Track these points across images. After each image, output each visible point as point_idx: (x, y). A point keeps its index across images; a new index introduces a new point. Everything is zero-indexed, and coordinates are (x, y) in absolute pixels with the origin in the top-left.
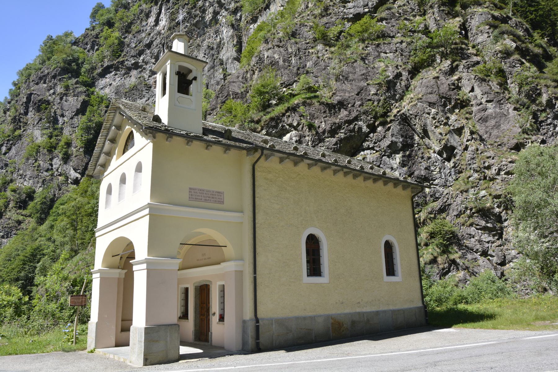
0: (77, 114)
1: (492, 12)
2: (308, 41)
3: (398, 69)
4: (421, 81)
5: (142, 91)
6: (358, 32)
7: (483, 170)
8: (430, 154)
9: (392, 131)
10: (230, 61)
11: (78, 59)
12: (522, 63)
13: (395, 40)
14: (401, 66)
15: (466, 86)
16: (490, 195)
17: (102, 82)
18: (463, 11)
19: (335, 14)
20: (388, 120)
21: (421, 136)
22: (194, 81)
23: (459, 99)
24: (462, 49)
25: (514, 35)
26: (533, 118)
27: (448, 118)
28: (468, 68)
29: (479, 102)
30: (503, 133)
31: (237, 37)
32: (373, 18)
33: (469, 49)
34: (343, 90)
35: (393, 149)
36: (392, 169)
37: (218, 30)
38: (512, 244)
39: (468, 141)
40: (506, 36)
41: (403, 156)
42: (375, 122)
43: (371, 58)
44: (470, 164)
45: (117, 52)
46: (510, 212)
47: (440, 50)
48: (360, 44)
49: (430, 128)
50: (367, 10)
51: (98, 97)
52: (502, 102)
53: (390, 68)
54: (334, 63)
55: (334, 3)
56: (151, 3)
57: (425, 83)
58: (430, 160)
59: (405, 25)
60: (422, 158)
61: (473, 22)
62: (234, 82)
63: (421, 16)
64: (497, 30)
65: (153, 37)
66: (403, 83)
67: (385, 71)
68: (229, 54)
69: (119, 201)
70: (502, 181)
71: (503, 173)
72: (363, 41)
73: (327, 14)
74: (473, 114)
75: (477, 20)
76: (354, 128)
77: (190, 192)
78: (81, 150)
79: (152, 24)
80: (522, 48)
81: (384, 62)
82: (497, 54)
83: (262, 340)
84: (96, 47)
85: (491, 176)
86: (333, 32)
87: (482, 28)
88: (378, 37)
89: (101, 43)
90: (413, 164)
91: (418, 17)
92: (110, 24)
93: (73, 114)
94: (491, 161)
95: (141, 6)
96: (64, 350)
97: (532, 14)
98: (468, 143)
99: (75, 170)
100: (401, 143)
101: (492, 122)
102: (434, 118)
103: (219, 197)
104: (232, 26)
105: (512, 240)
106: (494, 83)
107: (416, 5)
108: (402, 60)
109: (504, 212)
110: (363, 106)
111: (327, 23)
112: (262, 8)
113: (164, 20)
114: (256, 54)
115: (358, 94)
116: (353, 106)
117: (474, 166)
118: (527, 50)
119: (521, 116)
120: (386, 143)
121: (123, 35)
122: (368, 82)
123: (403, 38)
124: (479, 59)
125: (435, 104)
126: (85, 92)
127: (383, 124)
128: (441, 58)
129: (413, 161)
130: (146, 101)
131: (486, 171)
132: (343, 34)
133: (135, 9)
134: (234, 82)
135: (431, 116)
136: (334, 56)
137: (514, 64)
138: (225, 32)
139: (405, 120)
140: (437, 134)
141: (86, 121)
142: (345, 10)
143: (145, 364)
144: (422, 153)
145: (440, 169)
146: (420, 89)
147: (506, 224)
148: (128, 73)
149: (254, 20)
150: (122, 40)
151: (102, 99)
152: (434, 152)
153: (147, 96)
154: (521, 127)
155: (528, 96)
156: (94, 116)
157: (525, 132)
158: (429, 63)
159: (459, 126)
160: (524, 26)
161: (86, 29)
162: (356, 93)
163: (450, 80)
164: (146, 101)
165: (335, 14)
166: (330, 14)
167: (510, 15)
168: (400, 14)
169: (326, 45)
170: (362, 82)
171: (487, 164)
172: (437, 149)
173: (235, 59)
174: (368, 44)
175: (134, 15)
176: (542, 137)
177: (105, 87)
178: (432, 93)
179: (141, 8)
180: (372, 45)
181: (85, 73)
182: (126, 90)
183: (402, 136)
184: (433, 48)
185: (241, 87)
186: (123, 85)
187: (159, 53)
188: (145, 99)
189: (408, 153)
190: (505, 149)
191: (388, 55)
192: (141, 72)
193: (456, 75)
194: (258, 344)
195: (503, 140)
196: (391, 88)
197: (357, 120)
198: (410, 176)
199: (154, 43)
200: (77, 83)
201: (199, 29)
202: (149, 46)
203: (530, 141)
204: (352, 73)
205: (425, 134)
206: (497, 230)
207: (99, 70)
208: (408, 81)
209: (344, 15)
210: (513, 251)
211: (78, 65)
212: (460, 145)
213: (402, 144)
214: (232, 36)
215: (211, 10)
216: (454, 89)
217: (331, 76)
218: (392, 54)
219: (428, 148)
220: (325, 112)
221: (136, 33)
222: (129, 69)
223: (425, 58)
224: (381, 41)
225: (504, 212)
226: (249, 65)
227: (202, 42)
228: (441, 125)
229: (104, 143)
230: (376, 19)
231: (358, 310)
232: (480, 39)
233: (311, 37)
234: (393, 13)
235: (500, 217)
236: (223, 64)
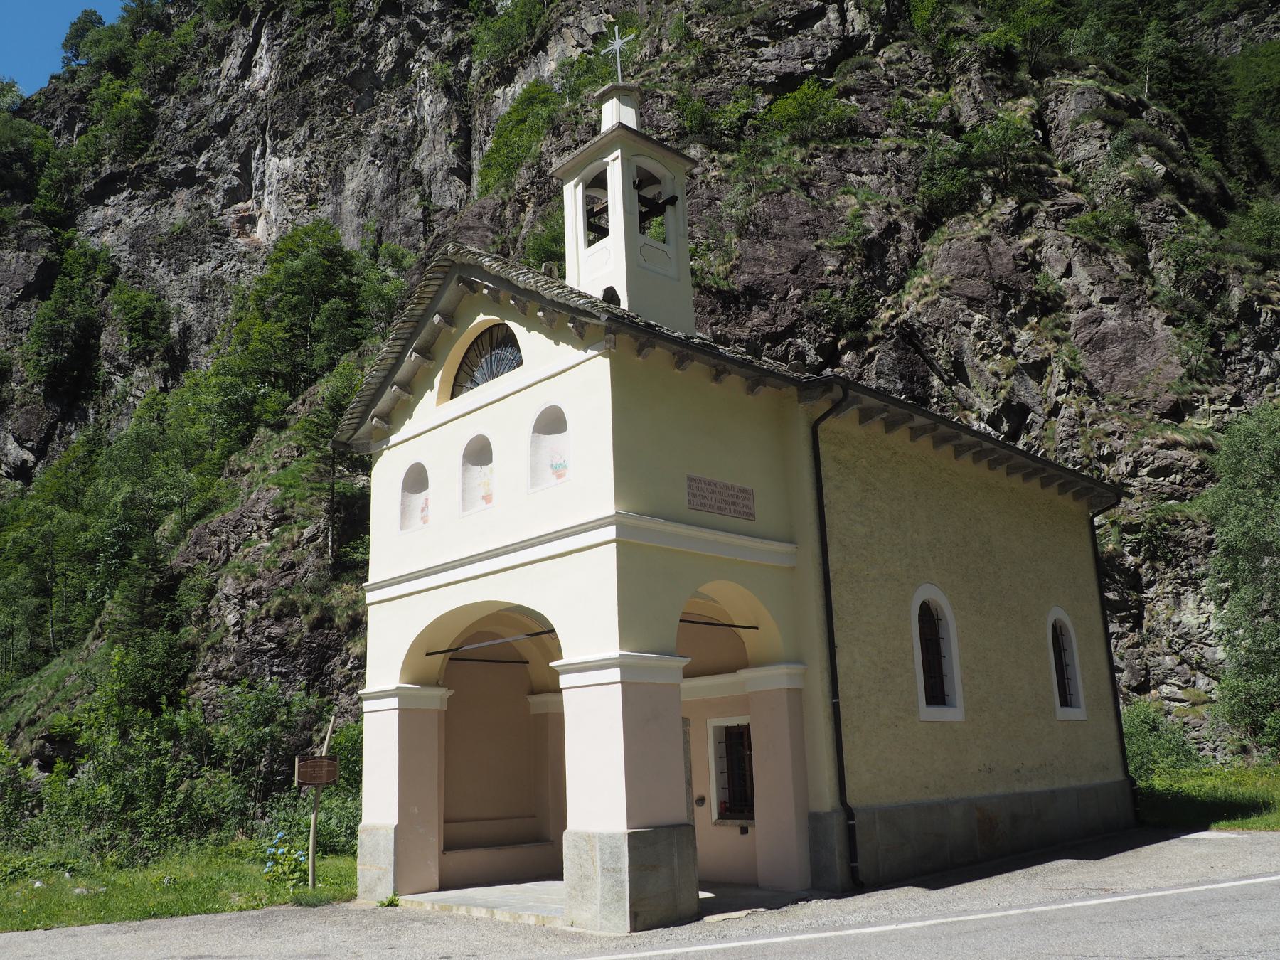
0: (25, 297)
1: (1107, 88)
2: (665, 135)
3: (891, 214)
4: (947, 245)
5: (204, 242)
6: (791, 120)
7: (1095, 463)
9: (879, 364)
10: (440, 175)
11: (30, 152)
12: (1181, 214)
13: (882, 144)
14: (897, 207)
15: (1053, 262)
16: (1114, 523)
17: (95, 216)
18: (1036, 83)
19: (732, 72)
20: (870, 336)
21: (946, 377)
22: (668, 207)
23: (1038, 293)
24: (1039, 173)
25: (1160, 147)
26: (1211, 344)
27: (1012, 338)
28: (1057, 220)
29: (1084, 301)
30: (1142, 376)
31: (459, 116)
32: (826, 86)
33: (1056, 175)
34: (759, 259)
37: (409, 98)
38: (1164, 642)
39: (1059, 393)
40: (1141, 148)
42: (836, 340)
44: (1065, 450)
45: (137, 141)
46: (1160, 565)
47: (990, 173)
48: (796, 148)
49: (970, 359)
50: (809, 67)
51: (85, 255)
52: (1137, 302)
53: (873, 211)
54: (733, 193)
55: (729, 46)
56: (232, 18)
59: (904, 109)
61: (1062, 110)
62: (469, 228)
63: (938, 87)
64: (1125, 132)
65: (234, 107)
66: (903, 249)
67: (861, 216)
68: (437, 159)
69: (464, 509)
70: (1142, 490)
71: (1144, 471)
72: (803, 141)
73: (712, 71)
74: (1072, 330)
75: (1073, 105)
76: (786, 352)
77: (689, 487)
78: (36, 390)
79: (233, 73)
80: (1179, 177)
81: (855, 195)
82: (1123, 189)
83: (862, 864)
84: (80, 125)
85: (1116, 479)
86: (731, 112)
87: (1085, 125)
88: (839, 135)
89: (94, 115)
91: (933, 93)
92: (118, 66)
93: (16, 295)
94: (1118, 444)
95: (201, 25)
96: (298, 902)
97: (1182, 98)
98: (1059, 399)
99: (20, 441)
101: (1116, 351)
102: (979, 336)
103: (745, 502)
104: (447, 90)
105: (1167, 633)
106: (1118, 257)
107: (928, 61)
108: (899, 192)
109: (1147, 564)
110: (807, 299)
111: (711, 93)
112: (527, 48)
113: (266, 64)
114: (530, 161)
115: (794, 272)
116: (783, 299)
117: (1076, 453)
118: (1190, 182)
119: (1183, 338)
121: (153, 96)
123: (900, 140)
124: (1080, 198)
125: (982, 302)
126: (49, 240)
127: (857, 346)
128: (994, 192)
130: (215, 268)
131: (1104, 466)
132: (750, 121)
133: (185, 30)
134: (469, 228)
135: (973, 331)
136: (733, 175)
137: (1162, 214)
138: (426, 102)
139: (909, 338)
140: (987, 373)
141: (53, 314)
142: (755, 64)
143: (634, 929)
146: (944, 265)
147: (1150, 593)
148: (167, 196)
149: (506, 77)
150: (151, 109)
151: (93, 261)
152: (980, 418)
153: (218, 255)
154: (1183, 365)
155: (1198, 292)
156: (72, 302)
157: (1193, 375)
158: (965, 203)
159: (1040, 357)
160: (1176, 127)
161: (53, 77)
162: (791, 267)
163: (1015, 246)
164: (215, 268)
165: (732, 72)
166: (720, 71)
167: (1145, 97)
168: (891, 81)
169: (711, 147)
170: (804, 240)
171: (1105, 450)
172: (987, 410)
173: (452, 171)
174: (816, 149)
175: (183, 46)
176: (1234, 390)
177: (103, 228)
178: (974, 276)
179: (202, 30)
180: (825, 152)
181: (48, 189)
182: (159, 240)
183: (902, 377)
184: (972, 167)
185: (488, 241)
186: (152, 226)
187: (250, 148)
188: (211, 264)
190: (1147, 414)
191: (865, 178)
192: (200, 194)
193: (1030, 234)
194: (853, 872)
195: (1142, 394)
196: (876, 259)
197: (794, 335)
199: (239, 122)
200: (27, 215)
201: (359, 91)
202: (223, 128)
203: (1206, 397)
204: (778, 218)
205: (958, 372)
206: (1131, 608)
207: (89, 185)
208: (915, 243)
210: (1167, 658)
211: (29, 168)
212: (1041, 403)
214: (447, 115)
215: (391, 45)
216: (1025, 269)
217: (725, 223)
218: (874, 177)
219: (965, 409)
220: (713, 312)
221: (189, 93)
222: (168, 187)
223: (954, 189)
224: (847, 144)
225: (1147, 564)
226: (509, 186)
227: (366, 126)
228: (995, 352)
229: (399, 360)
230: (833, 90)
231: (1018, 788)
232: (1082, 151)
233: (673, 125)
235: (1138, 576)
236: (421, 184)
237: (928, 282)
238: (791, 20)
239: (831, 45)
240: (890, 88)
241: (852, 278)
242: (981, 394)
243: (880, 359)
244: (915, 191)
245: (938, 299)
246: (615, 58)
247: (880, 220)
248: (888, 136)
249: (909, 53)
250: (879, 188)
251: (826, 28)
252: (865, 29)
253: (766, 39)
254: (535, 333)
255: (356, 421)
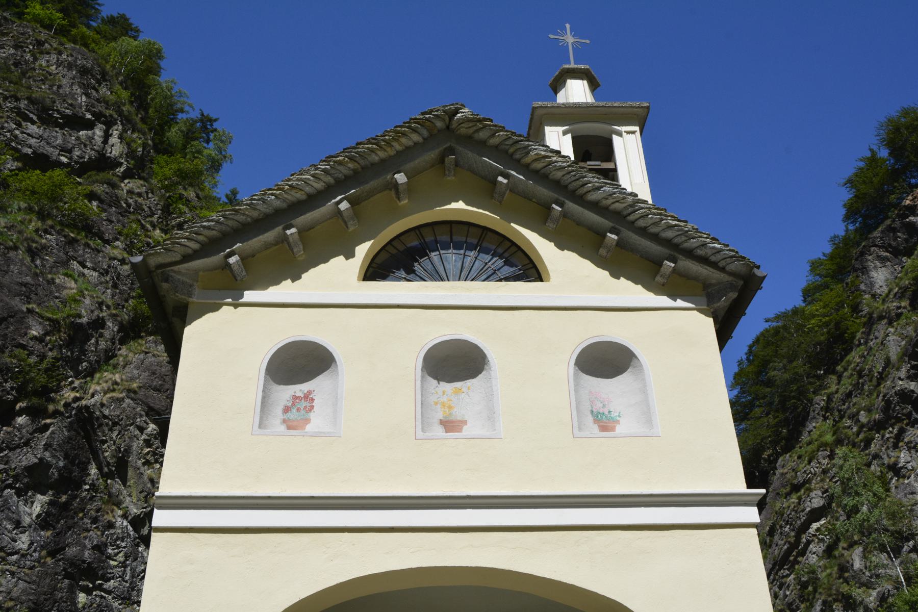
8: (114, 517)
14: (108, 307)
20: (51, 408)
21: (106, 469)
35: (34, 479)
36: (18, 524)
41: (51, 503)
42: (16, 400)
43: (50, 260)
50: (64, 160)
53: (87, 301)
57: (151, 365)
58: (112, 531)
60: (95, 520)
63: (162, 230)
66: (103, 345)
67: (75, 301)
88: (73, 226)
90: (69, 528)
100: (59, 470)
107: (159, 207)
108: (113, 296)
120: (26, 458)
122: (30, 306)
127: (35, 413)
129: (70, 522)
139: (86, 423)
140: (146, 478)
144: (98, 511)
145: (127, 557)
146: (136, 372)
152: (125, 516)
170: (18, 299)
174: (52, 227)
180: (58, 233)
183: (66, 457)
189: (64, 498)
191: (86, 271)
198: (52, 554)
208: (113, 343)
209: (11, 140)
213: (60, 474)
218: (96, 274)
234: (117, 197)
237: (119, 380)
238: (64, 116)
239: (89, 154)
240: (126, 211)
241: (51, 350)
242: (134, 494)
243: (53, 433)
244: (127, 301)
245: (123, 399)
246: (557, 33)
247: (92, 311)
248: (117, 247)
249: (147, 193)
250: (96, 285)
251: (91, 139)
252: (121, 156)
253: (35, 118)
254: (566, 251)
255: (195, 246)
